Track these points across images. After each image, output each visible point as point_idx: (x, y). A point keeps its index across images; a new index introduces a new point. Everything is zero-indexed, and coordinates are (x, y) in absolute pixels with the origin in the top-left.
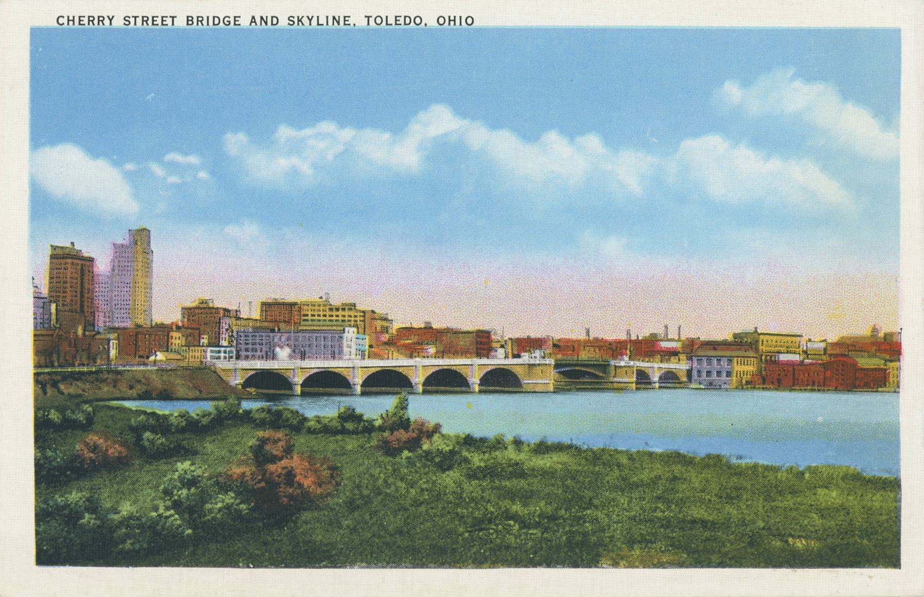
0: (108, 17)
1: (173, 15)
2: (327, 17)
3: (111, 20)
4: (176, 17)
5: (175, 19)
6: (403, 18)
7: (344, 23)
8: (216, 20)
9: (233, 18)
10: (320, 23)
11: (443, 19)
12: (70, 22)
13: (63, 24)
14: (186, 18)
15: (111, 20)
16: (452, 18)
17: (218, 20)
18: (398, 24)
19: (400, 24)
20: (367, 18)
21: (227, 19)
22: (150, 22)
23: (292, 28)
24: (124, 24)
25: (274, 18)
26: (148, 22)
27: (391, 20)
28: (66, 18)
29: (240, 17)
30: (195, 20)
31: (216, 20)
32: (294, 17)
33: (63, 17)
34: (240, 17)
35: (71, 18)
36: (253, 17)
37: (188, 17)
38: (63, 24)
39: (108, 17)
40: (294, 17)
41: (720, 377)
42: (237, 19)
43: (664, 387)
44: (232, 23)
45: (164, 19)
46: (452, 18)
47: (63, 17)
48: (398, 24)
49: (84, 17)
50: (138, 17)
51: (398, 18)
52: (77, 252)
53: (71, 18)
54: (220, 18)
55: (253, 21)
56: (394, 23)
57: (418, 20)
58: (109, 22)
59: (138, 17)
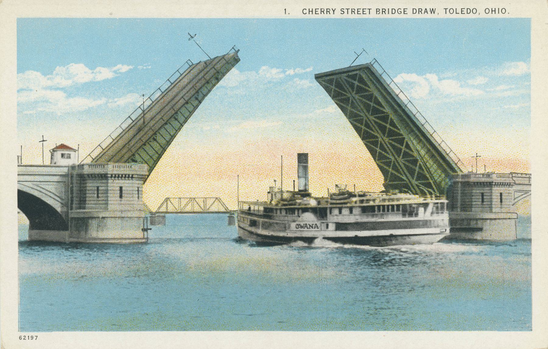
0: (332, 9)
1: (446, 8)
2: (499, 9)
3: (334, 11)
4: (371, 9)
5: (370, 10)
6: (362, 10)
7: (462, 12)
8: (394, 11)
9: (382, 10)
10: (457, 12)
11: (504, 9)
12: (494, 10)
13: (306, 13)
14: (461, 10)
15: (334, 11)
16: (493, 10)
17: (470, 10)
18: (364, 14)
19: (360, 14)
20: (445, 10)
21: (399, 10)
22: (356, 12)
23: (394, 17)
24: (341, 13)
25: (414, 9)
26: (324, 12)
27: (459, 11)
28: (308, 10)
29: (407, 9)
30: (381, 11)
31: (394, 11)
32: (344, 9)
33: (306, 9)
34: (407, 9)
35: (311, 10)
36: (426, 9)
37: (377, 9)
38: (306, 13)
39: (332, 9)
40: (344, 9)
41: (84, 208)
42: (405, 10)
43: (18, 158)
44: (403, 12)
45: (364, 10)
46: (493, 10)
47: (306, 9)
48: (364, 14)
49: (318, 9)
50: (349, 9)
51: (463, 10)
52: (257, 238)
53: (311, 10)
54: (471, 9)
55: (426, 11)
56: (460, 13)
57: (474, 11)
58: (333, 12)
59: (349, 9)
